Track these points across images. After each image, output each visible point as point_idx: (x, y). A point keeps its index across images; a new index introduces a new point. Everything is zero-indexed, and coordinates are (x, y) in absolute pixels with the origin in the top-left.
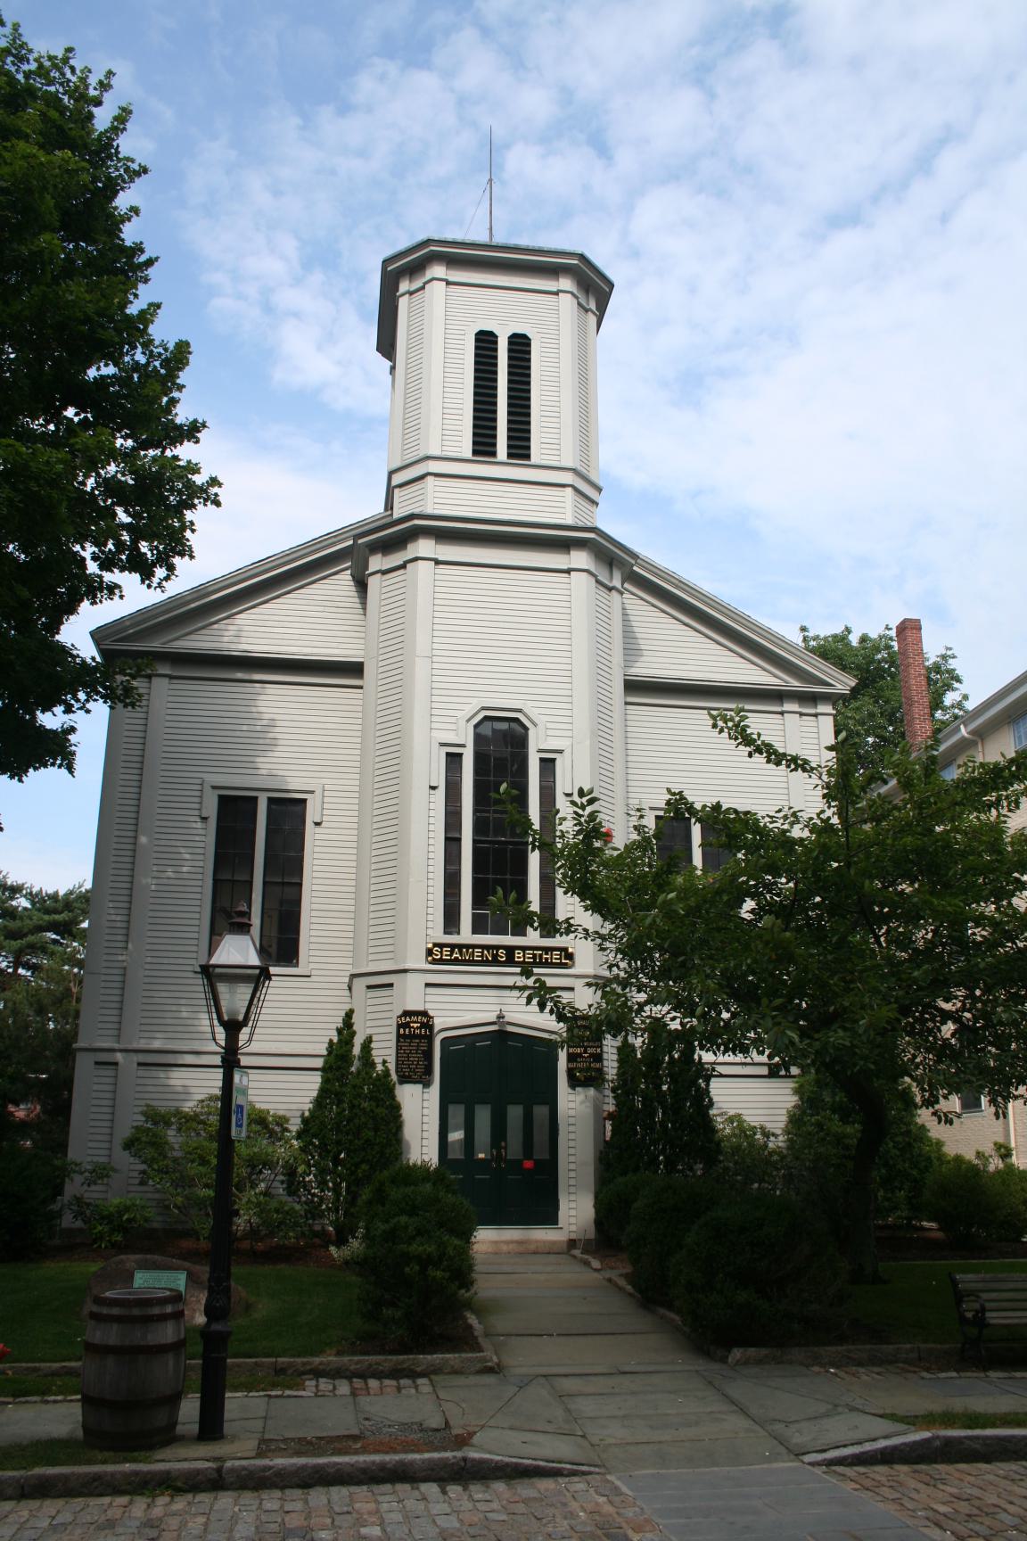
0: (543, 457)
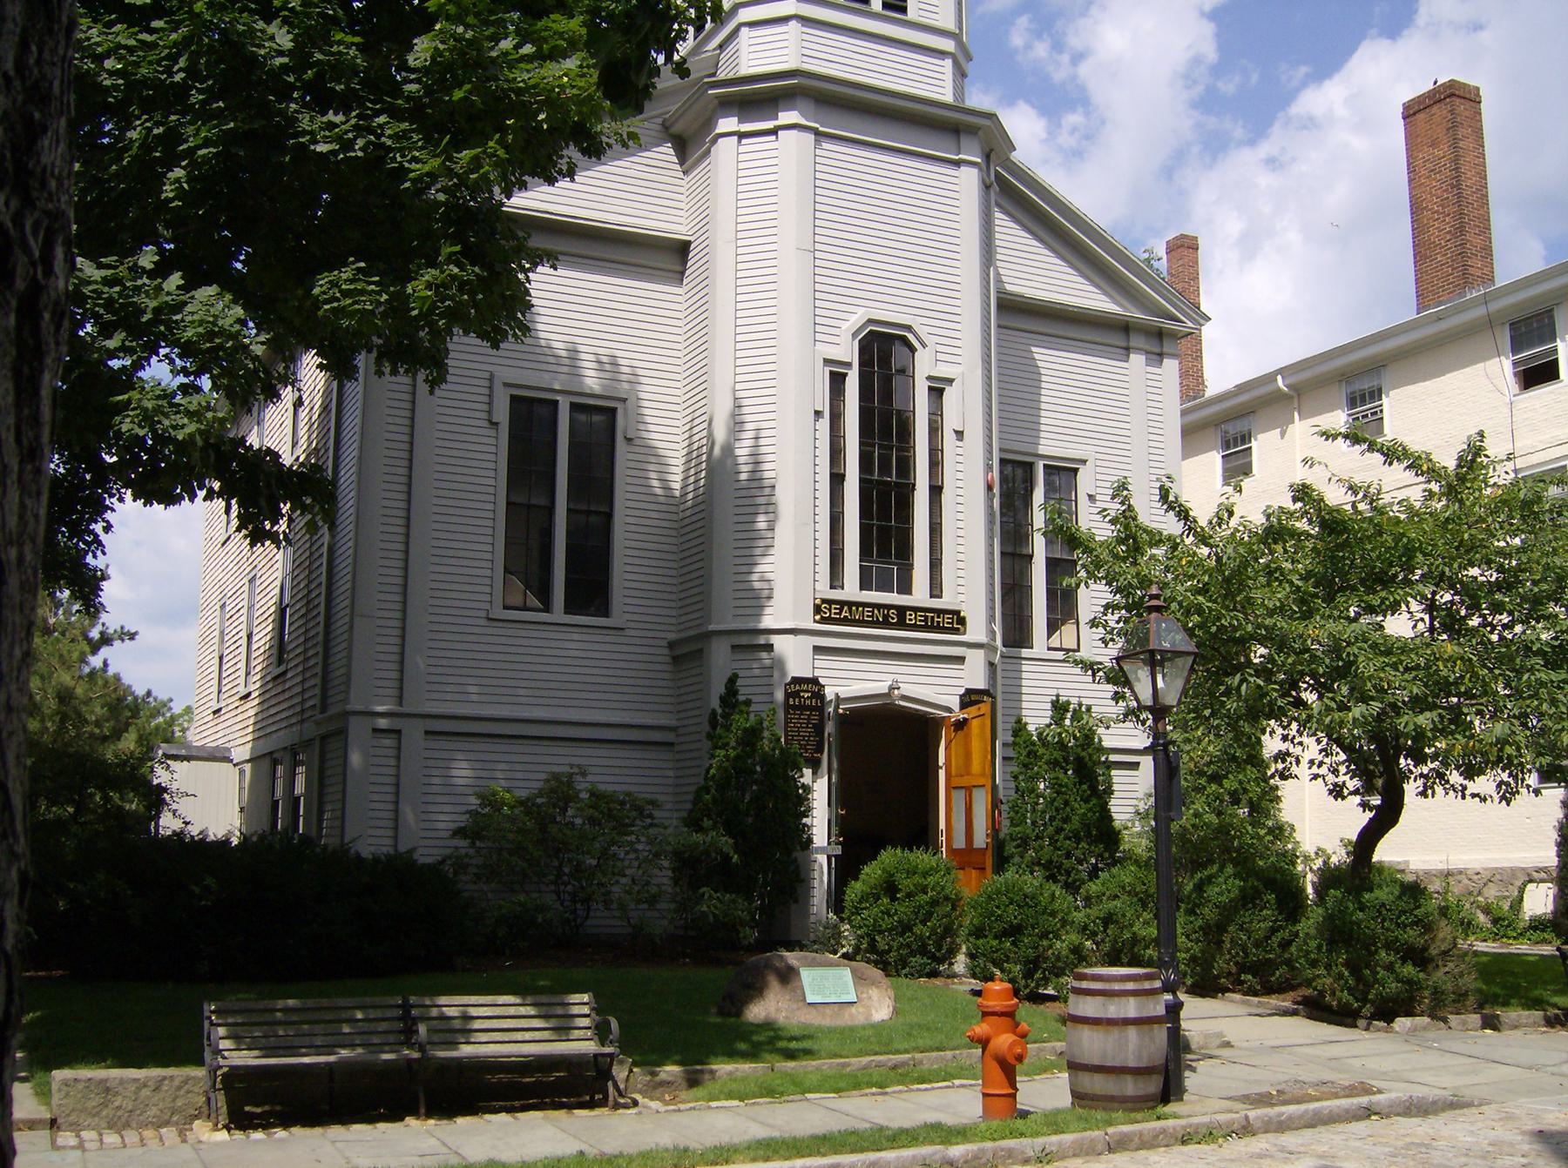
0: (921, 13)
